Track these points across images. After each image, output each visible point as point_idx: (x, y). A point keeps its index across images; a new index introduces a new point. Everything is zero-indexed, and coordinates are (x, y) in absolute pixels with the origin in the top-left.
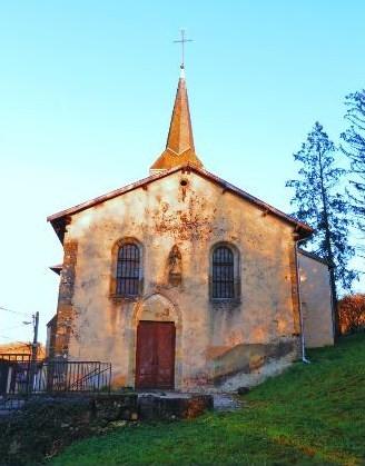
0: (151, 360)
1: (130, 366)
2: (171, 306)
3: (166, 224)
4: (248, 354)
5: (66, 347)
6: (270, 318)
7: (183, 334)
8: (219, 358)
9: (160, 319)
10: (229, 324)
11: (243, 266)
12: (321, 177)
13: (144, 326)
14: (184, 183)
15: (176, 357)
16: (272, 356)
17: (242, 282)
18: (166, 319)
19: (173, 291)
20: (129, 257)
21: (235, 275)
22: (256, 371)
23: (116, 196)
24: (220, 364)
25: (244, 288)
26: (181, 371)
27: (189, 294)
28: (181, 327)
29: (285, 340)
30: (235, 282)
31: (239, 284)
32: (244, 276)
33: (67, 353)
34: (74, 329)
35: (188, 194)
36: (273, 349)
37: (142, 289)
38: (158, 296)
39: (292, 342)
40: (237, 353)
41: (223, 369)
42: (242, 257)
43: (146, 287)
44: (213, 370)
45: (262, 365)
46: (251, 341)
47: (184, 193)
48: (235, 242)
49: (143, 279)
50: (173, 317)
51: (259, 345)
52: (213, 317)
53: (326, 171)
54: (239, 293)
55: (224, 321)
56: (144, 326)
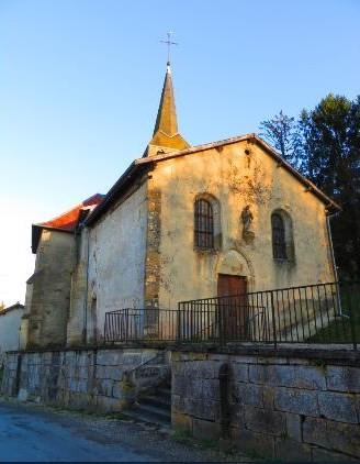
5: (156, 296)
11: (295, 232)
18: (242, 274)
19: (246, 249)
33: (157, 301)
49: (220, 235)
52: (277, 273)
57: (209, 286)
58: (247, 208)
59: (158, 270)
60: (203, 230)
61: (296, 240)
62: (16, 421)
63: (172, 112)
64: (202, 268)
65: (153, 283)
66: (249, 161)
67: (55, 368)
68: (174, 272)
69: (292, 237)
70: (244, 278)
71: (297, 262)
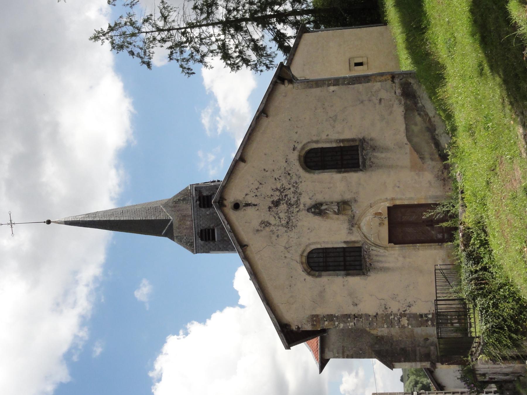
0: (429, 228)
1: (435, 249)
2: (372, 211)
3: (284, 222)
4: (416, 129)
5: (421, 316)
6: (468, 82)
7: (399, 196)
8: (422, 158)
9: (386, 222)
10: (386, 149)
11: (324, 137)
12: (169, 30)
13: (394, 239)
14: (236, 206)
15: (423, 202)
16: (416, 103)
17: (342, 137)
18: (385, 214)
19: (357, 210)
20: (321, 260)
21: (334, 145)
22: (433, 119)
23: (360, 57)
24: (427, 156)
25: (348, 135)
26: (437, 197)
27: (357, 193)
28: (393, 199)
29: (399, 91)
30: (342, 145)
31: (343, 141)
32: (335, 136)
33: (426, 315)
34: (401, 311)
35: (250, 199)
36: (408, 102)
37: (354, 242)
38: (362, 224)
39: (401, 84)
40: (416, 140)
41: (432, 154)
42: (315, 139)
43: (353, 238)
44: (434, 163)
45: (427, 115)
46: (403, 128)
47: (247, 205)
48: (299, 147)
49: (345, 242)
50: (383, 207)
51: (406, 117)
52: (379, 167)
53: (161, 24)
54: (353, 140)
55: (383, 155)
56: (394, 239)
57: (404, 257)
58: (159, 41)
59: (395, 315)
60: (342, 259)
61: (335, 136)
62: (150, 208)
63: (70, 219)
64: (387, 265)
65: (408, 320)
66: (247, 205)
67: (238, 4)
68: (394, 297)
69: (331, 142)
70: (389, 208)
71: (360, 136)
